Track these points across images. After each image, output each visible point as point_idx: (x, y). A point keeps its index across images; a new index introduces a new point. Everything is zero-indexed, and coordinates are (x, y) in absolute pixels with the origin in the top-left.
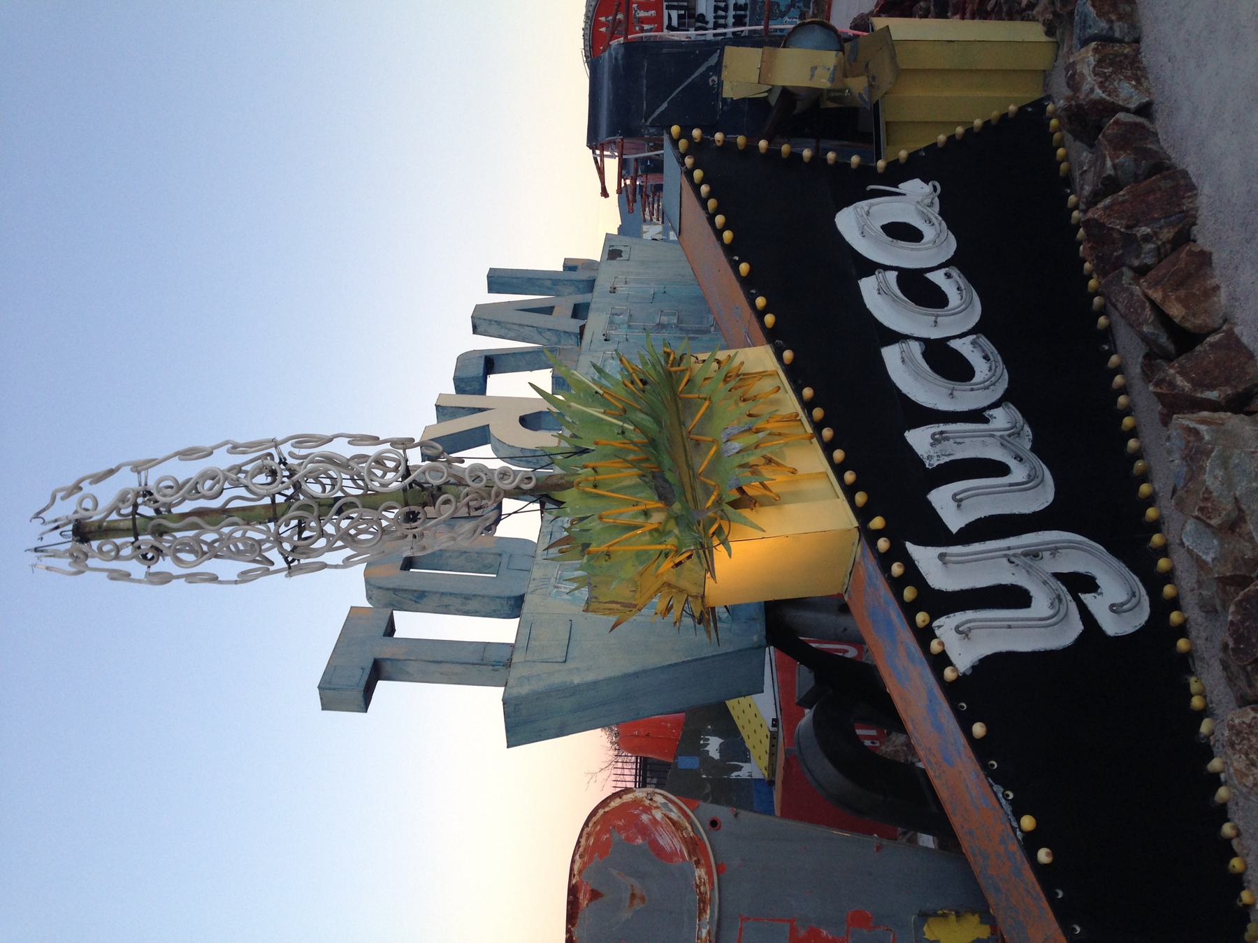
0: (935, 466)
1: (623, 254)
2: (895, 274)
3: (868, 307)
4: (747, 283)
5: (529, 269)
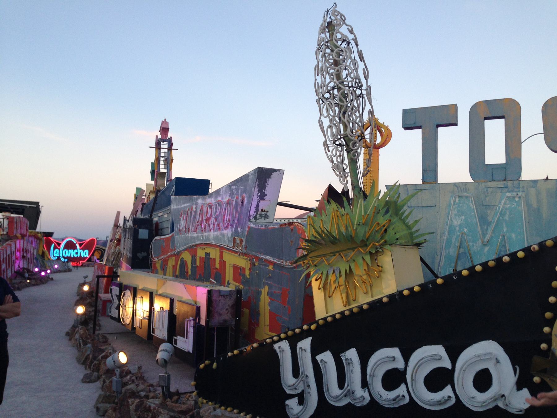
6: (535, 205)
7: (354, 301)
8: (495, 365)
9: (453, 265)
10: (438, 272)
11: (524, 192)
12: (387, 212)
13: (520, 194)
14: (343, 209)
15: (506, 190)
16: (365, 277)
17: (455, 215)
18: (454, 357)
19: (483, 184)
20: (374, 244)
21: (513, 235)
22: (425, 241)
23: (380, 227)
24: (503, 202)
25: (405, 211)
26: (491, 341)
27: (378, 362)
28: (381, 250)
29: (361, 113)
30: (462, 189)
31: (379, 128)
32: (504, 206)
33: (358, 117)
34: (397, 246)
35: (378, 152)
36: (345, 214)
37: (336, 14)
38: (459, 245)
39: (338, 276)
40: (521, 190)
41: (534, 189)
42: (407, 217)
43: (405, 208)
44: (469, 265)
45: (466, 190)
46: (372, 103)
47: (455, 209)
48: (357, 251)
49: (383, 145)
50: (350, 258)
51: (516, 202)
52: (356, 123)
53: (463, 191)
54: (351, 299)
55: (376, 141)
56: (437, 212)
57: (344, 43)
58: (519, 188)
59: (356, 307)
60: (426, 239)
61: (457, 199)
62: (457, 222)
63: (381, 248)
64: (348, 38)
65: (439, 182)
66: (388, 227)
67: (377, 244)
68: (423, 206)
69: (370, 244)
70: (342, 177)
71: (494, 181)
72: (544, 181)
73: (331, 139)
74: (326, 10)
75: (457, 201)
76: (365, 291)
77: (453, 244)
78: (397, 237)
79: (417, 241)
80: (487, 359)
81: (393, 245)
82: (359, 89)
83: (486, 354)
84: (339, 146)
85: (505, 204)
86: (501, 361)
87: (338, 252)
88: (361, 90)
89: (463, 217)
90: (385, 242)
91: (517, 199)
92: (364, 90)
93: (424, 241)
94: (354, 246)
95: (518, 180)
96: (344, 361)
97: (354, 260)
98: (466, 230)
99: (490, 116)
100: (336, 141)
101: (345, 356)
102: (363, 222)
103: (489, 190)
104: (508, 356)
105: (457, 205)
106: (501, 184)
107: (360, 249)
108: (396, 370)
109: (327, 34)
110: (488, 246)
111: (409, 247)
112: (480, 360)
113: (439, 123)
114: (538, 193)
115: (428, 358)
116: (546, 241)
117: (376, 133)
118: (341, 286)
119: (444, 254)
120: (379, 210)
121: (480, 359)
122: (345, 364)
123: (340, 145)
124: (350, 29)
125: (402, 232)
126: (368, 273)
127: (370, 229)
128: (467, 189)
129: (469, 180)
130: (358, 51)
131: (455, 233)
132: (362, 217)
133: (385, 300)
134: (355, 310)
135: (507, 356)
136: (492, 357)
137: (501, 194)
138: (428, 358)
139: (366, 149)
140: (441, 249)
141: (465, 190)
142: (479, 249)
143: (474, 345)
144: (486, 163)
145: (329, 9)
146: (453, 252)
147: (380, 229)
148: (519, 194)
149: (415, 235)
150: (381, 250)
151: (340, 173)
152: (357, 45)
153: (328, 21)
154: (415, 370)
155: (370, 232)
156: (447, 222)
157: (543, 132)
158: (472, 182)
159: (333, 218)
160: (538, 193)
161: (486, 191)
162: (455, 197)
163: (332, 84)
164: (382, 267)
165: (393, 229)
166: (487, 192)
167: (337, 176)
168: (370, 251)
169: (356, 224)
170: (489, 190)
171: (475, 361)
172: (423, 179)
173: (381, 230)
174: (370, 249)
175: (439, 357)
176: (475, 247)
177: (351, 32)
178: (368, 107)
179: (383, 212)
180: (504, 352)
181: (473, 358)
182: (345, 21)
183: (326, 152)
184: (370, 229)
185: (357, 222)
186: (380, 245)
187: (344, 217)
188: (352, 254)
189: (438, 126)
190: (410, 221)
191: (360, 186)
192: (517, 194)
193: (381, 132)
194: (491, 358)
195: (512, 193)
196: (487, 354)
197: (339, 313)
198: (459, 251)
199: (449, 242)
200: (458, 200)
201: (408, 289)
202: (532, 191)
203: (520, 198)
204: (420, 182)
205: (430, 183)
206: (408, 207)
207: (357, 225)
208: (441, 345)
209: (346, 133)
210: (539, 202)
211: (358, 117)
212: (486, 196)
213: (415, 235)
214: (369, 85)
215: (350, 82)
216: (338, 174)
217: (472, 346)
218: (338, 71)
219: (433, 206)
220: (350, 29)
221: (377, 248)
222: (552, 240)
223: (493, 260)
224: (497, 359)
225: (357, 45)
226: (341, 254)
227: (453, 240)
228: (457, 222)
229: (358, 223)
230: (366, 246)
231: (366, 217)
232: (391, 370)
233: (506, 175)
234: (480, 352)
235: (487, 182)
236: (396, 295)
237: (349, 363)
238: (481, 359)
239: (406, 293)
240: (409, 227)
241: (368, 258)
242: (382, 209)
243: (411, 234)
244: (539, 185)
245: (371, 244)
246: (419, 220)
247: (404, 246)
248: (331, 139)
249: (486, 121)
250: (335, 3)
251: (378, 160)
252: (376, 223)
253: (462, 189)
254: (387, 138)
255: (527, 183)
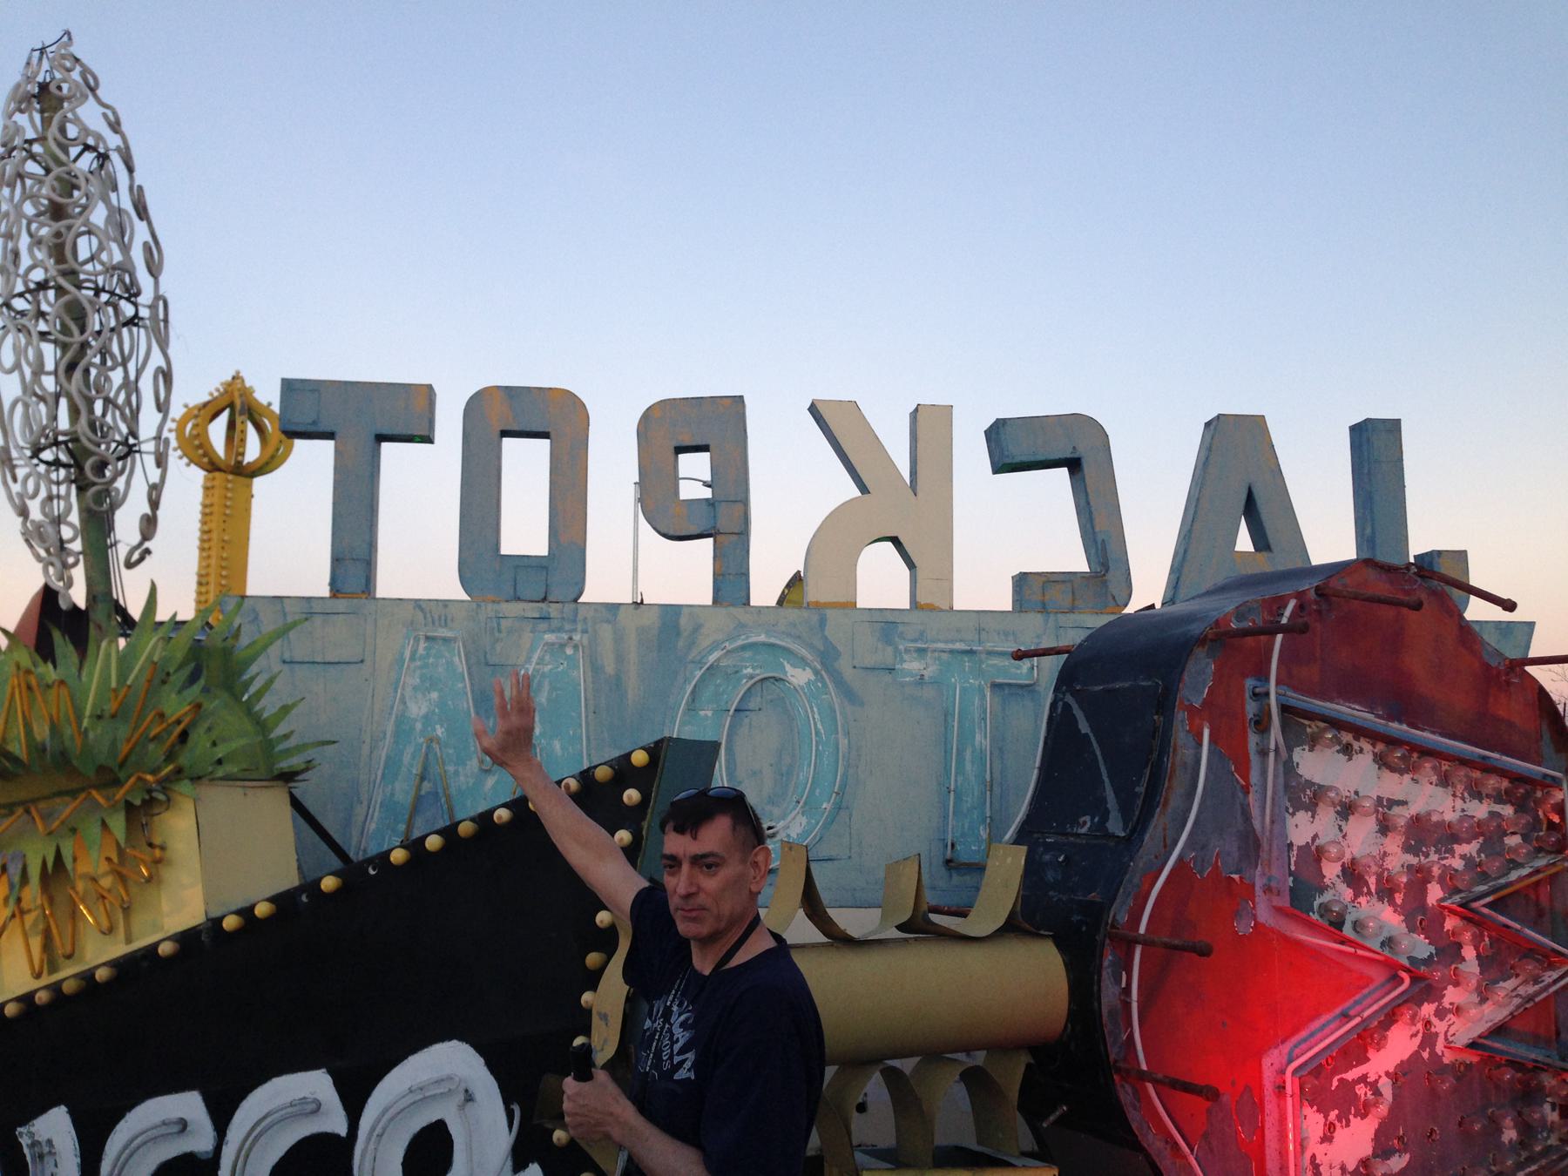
0: (20, 1140)
1: (807, 680)
2: (342, 1129)
3: (411, 1058)
4: (246, 913)
5: (1407, 490)
6: (610, 669)
7: (69, 957)
8: (461, 1107)
9: (402, 827)
10: (359, 849)
11: (587, 632)
12: (193, 678)
13: (577, 637)
14: (50, 666)
15: (543, 625)
16: (106, 882)
17: (415, 688)
18: (354, 1099)
19: (490, 606)
20: (140, 779)
21: (557, 745)
22: (309, 766)
23: (164, 725)
24: (535, 659)
25: (253, 679)
26: (455, 1043)
27: (137, 1137)
28: (161, 797)
29: (132, 376)
30: (436, 617)
31: (257, 416)
32: (538, 667)
33: (57, 396)
34: (216, 782)
35: (249, 486)
36: (53, 683)
37: (68, 64)
38: (419, 772)
39: (16, 879)
40: (580, 627)
41: (610, 626)
42: (259, 694)
43: (254, 669)
44: (442, 823)
45: (446, 620)
46: (171, 352)
47: (414, 671)
48: (85, 799)
49: (264, 467)
50: (57, 823)
51: (568, 658)
52: (116, 406)
53: (437, 623)
54: (60, 948)
55: (243, 454)
56: (366, 680)
57: (89, 157)
58: (575, 621)
59: (75, 976)
60: (310, 761)
61: (422, 645)
62: (417, 709)
63: (164, 790)
64: (105, 142)
65: (379, 595)
66: (193, 724)
67: (149, 778)
68: (327, 660)
69: (129, 777)
70: (52, 564)
71: (518, 599)
72: (633, 606)
73: (22, 443)
74: (40, 46)
75: (421, 651)
76: (105, 924)
77: (404, 769)
78: (220, 755)
79: (284, 765)
80: (441, 1094)
81: (205, 780)
82: (128, 299)
83: (438, 1082)
84: (53, 468)
85: (541, 661)
86: (478, 1096)
87: (22, 803)
88: (135, 305)
89: (435, 695)
90: (179, 771)
91: (569, 651)
92: (144, 306)
93: (303, 766)
94: (74, 785)
95: (575, 600)
96: (26, 1151)
97: (74, 830)
98: (440, 731)
99: (516, 427)
100: (44, 449)
101: (31, 1135)
102: (113, 710)
103: (504, 623)
104: (496, 1078)
105: (420, 659)
106: (532, 610)
107: (94, 793)
108: (188, 1159)
109: (37, 117)
110: (494, 775)
111: (254, 783)
112: (421, 1100)
113: (386, 431)
114: (619, 638)
115: (283, 1112)
116: (596, 767)
117: (243, 432)
118: (29, 911)
119: (378, 797)
120: (168, 674)
121: (421, 1096)
122: (29, 1159)
123: (57, 463)
124: (112, 118)
125: (236, 739)
126: (119, 869)
127: (136, 728)
128: (449, 618)
129: (457, 593)
130: (131, 188)
131: (413, 738)
132: (112, 695)
133: (166, 949)
134: (69, 988)
135: (492, 1078)
136: (453, 1087)
137: (531, 635)
138: (283, 1112)
139: (211, 475)
140: (372, 785)
141: (443, 622)
142: (471, 781)
143: (410, 1058)
144: (504, 550)
145: (47, 44)
146: (403, 792)
147: (164, 730)
148: (574, 637)
149: (281, 747)
150: (161, 797)
151: (47, 551)
152: (130, 170)
153: (40, 79)
154: (243, 1153)
155: (134, 740)
156: (392, 708)
157: (681, 481)
158: (468, 601)
159: (13, 695)
160: (619, 638)
161: (496, 625)
162: (417, 639)
163: (38, 275)
164: (163, 848)
165: (209, 729)
166: (499, 631)
167: (38, 558)
168: (129, 799)
169: (88, 713)
170: (504, 623)
171: (409, 1102)
172: (333, 583)
173: (170, 734)
174: (125, 794)
175: (314, 1106)
176: (462, 778)
177: (115, 126)
178: (157, 360)
179: (179, 678)
180: (485, 1068)
181: (404, 1097)
182: (99, 92)
183: (5, 483)
184: (136, 728)
185: (94, 705)
186: (159, 782)
187: (53, 693)
188: (66, 809)
189: (382, 438)
190: (268, 706)
191: (115, 596)
192: (571, 638)
193: (260, 429)
194: (450, 1090)
195: (559, 635)
196: (443, 1080)
197: (18, 999)
198: (419, 788)
199: (392, 764)
200: (425, 648)
201: (239, 912)
202: (606, 632)
203: (576, 647)
204: (324, 591)
205: (351, 596)
206: (284, 662)
207: (91, 716)
208: (324, 1070)
209: (73, 429)
210: (620, 658)
211: (57, 396)
212: (497, 640)
213: (281, 747)
214: (161, 293)
215: (100, 274)
216: (43, 553)
217: (406, 1061)
218: (58, 234)
219: (356, 663)
220: (112, 118)
221: (149, 791)
222: (611, 767)
223: (472, 819)
224: (466, 1091)
225: (130, 170)
226: (33, 810)
227: (406, 758)
228: (420, 708)
229: (99, 713)
230: (117, 783)
231: (122, 694)
232: (176, 1159)
233: (547, 586)
234: (424, 1077)
235: (499, 602)
236: (201, 931)
237: (41, 1156)
238: (425, 1098)
239: (230, 923)
240: (262, 726)
241: (118, 824)
242: (176, 671)
243: (269, 745)
244: (622, 614)
245: (132, 780)
246: (294, 705)
247: (238, 783)
248: (22, 443)
249: (506, 441)
250: (68, 33)
251: (248, 510)
252: (153, 713)
253: (436, 617)
254: (278, 450)
255: (596, 610)
